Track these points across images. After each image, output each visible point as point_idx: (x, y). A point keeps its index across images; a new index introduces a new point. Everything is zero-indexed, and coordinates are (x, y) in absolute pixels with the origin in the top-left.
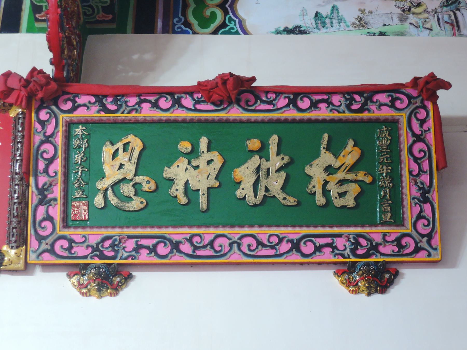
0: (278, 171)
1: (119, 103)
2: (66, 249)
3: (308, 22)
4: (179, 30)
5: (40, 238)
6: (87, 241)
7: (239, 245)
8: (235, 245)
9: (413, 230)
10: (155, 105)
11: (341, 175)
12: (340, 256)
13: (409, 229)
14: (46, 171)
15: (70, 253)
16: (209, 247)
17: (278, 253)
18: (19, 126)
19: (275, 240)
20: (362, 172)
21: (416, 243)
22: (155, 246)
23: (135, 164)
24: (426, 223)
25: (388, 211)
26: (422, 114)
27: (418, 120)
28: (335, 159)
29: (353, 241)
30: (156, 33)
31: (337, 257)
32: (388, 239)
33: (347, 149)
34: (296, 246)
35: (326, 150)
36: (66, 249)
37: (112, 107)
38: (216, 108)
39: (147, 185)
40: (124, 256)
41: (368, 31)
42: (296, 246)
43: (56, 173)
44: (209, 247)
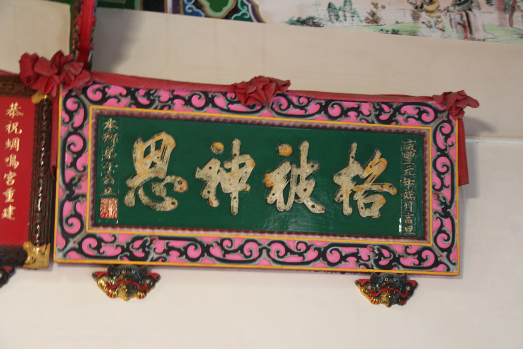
0: (308, 178)
1: (152, 97)
2: (95, 249)
3: (321, 13)
4: (190, 11)
5: (67, 236)
6: (117, 241)
7: (268, 251)
8: (264, 251)
9: (434, 244)
10: (188, 102)
11: (367, 186)
12: (364, 267)
13: (430, 243)
14: (73, 164)
15: (99, 252)
16: (239, 252)
17: (306, 260)
18: (44, 114)
19: (302, 247)
20: (387, 184)
21: (436, 257)
22: (186, 248)
23: (168, 163)
24: (446, 237)
25: (410, 224)
26: (447, 129)
27: (443, 134)
28: (362, 169)
29: (377, 252)
30: (167, 12)
31: (361, 267)
32: (409, 251)
33: (374, 160)
34: (322, 254)
35: (355, 160)
36: (95, 249)
37: (144, 101)
38: (249, 110)
39: (181, 186)
40: (154, 258)
41: (381, 28)
42: (322, 254)
43: (85, 168)
44: (239, 252)
